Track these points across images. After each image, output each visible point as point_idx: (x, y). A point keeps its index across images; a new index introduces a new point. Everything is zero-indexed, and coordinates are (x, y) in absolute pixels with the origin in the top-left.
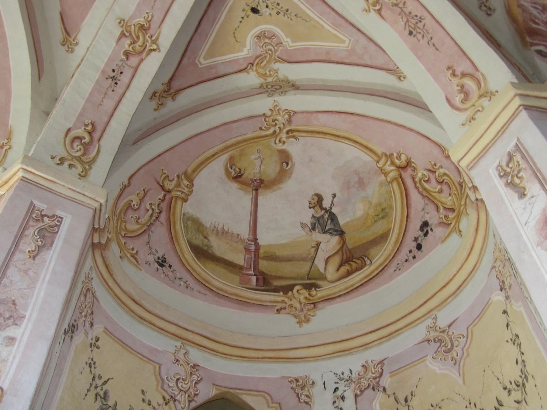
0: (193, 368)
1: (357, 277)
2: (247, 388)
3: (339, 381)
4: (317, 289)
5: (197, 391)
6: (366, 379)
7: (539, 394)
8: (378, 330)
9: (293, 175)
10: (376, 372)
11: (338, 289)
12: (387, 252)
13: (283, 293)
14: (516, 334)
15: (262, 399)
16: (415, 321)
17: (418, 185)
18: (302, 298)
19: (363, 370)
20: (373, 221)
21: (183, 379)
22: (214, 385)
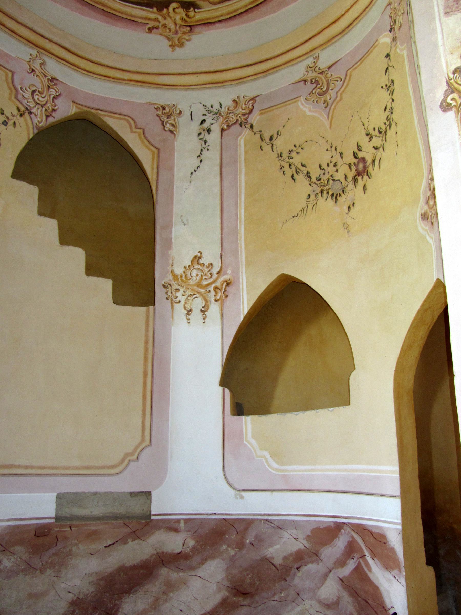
0: (51, 81)
2: (110, 110)
4: (196, 10)
5: (55, 106)
6: (234, 115)
7: (397, 141)
8: (255, 64)
10: (246, 108)
11: (220, 13)
13: (157, 10)
14: (392, 80)
15: (126, 123)
16: (296, 59)
18: (178, 18)
19: (234, 104)
21: (39, 92)
22: (74, 102)
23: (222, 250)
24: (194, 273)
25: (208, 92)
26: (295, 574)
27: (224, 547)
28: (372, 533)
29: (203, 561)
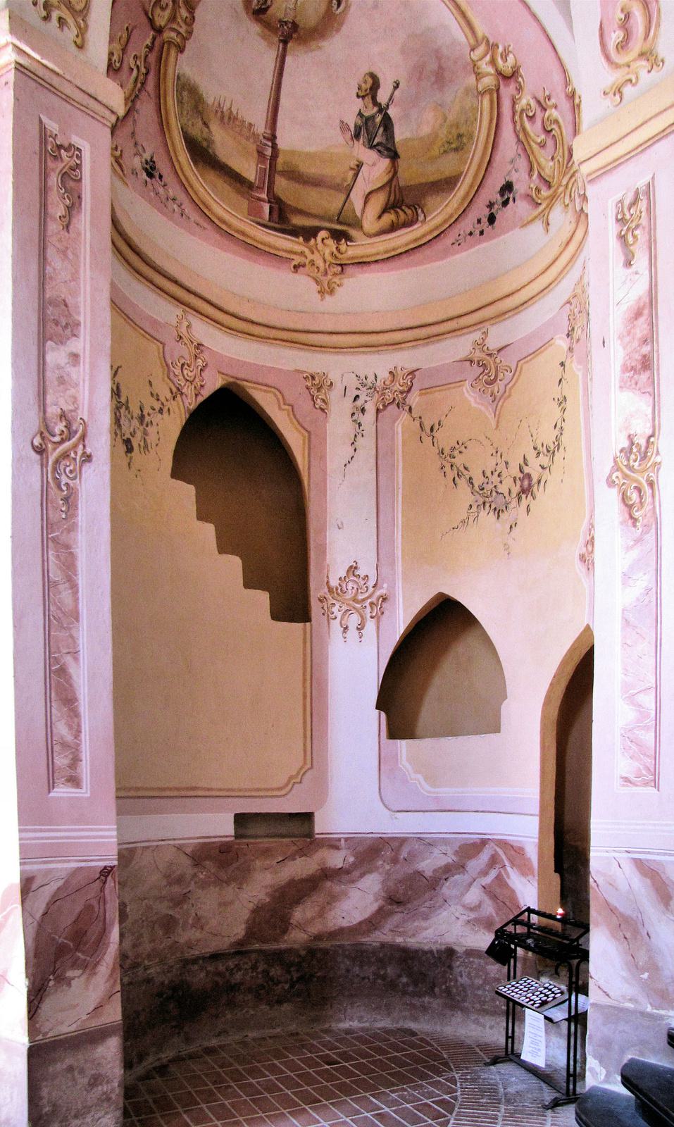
1: (403, 238)
3: (361, 387)
4: (349, 243)
9: (344, 29)
12: (449, 210)
17: (517, 118)
18: (327, 252)
20: (442, 151)
22: (219, 372)
23: (378, 560)
24: (350, 585)
25: (363, 358)
26: (443, 884)
27: (380, 863)
28: (512, 846)
29: (362, 875)
